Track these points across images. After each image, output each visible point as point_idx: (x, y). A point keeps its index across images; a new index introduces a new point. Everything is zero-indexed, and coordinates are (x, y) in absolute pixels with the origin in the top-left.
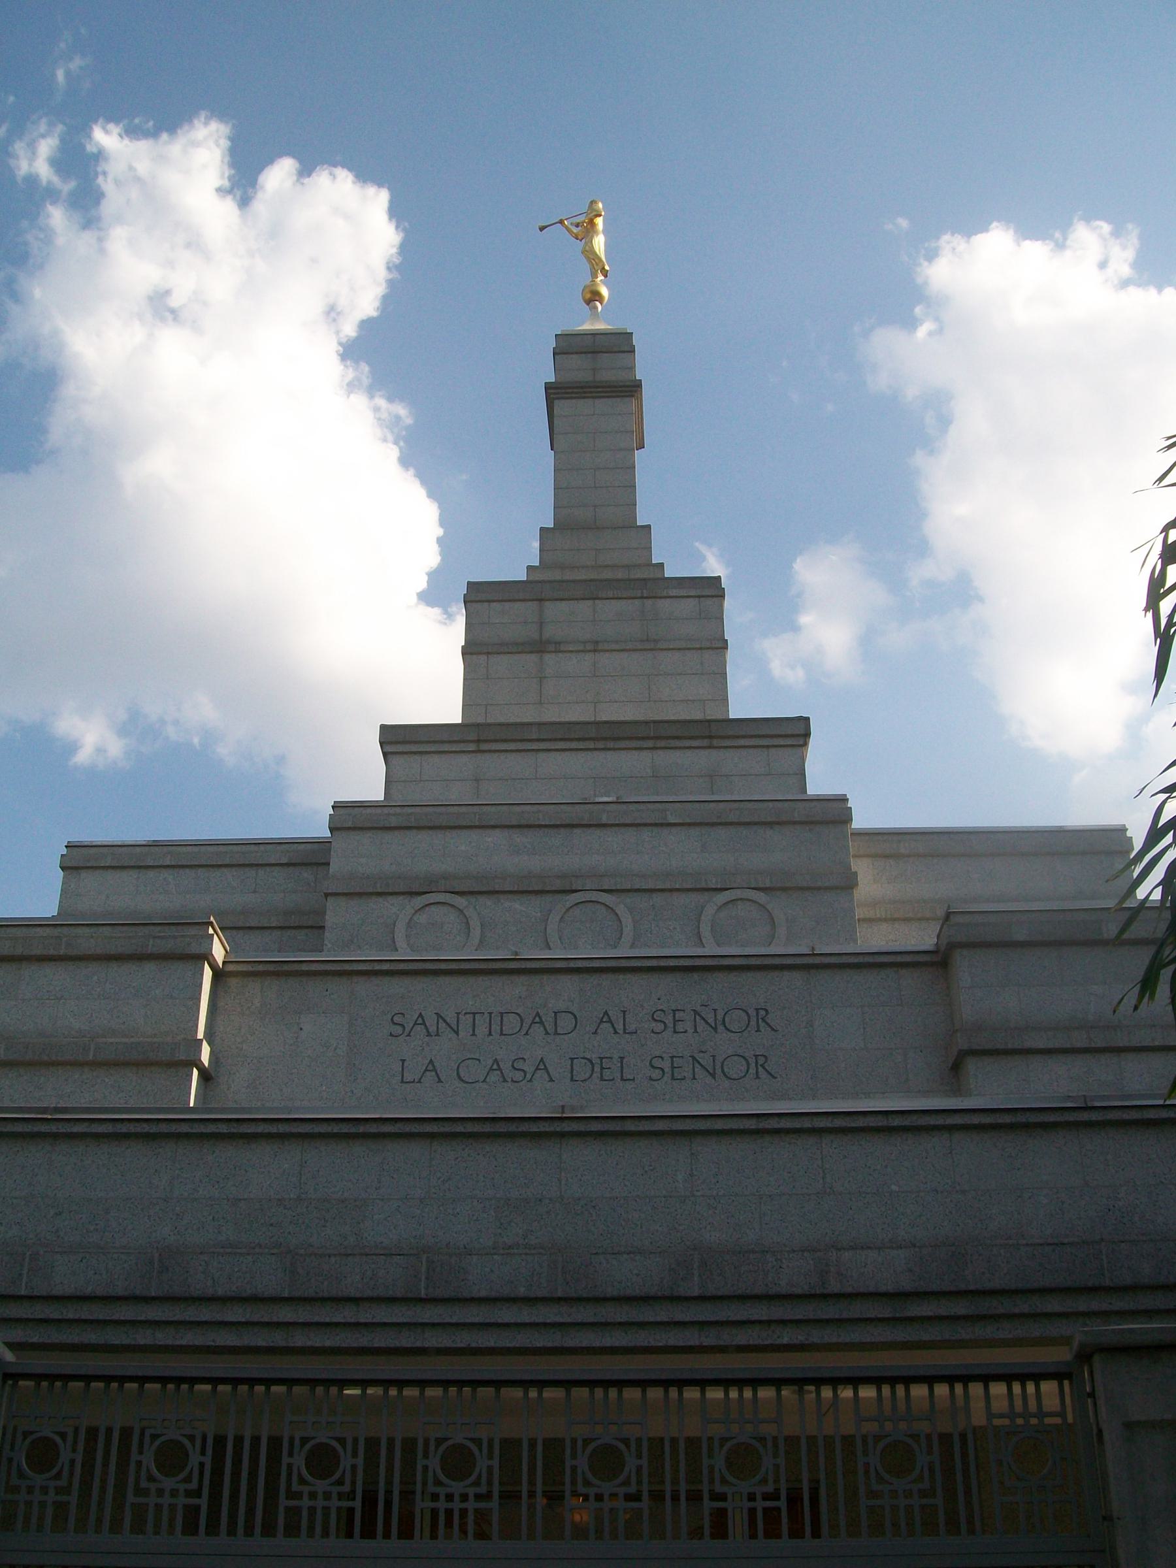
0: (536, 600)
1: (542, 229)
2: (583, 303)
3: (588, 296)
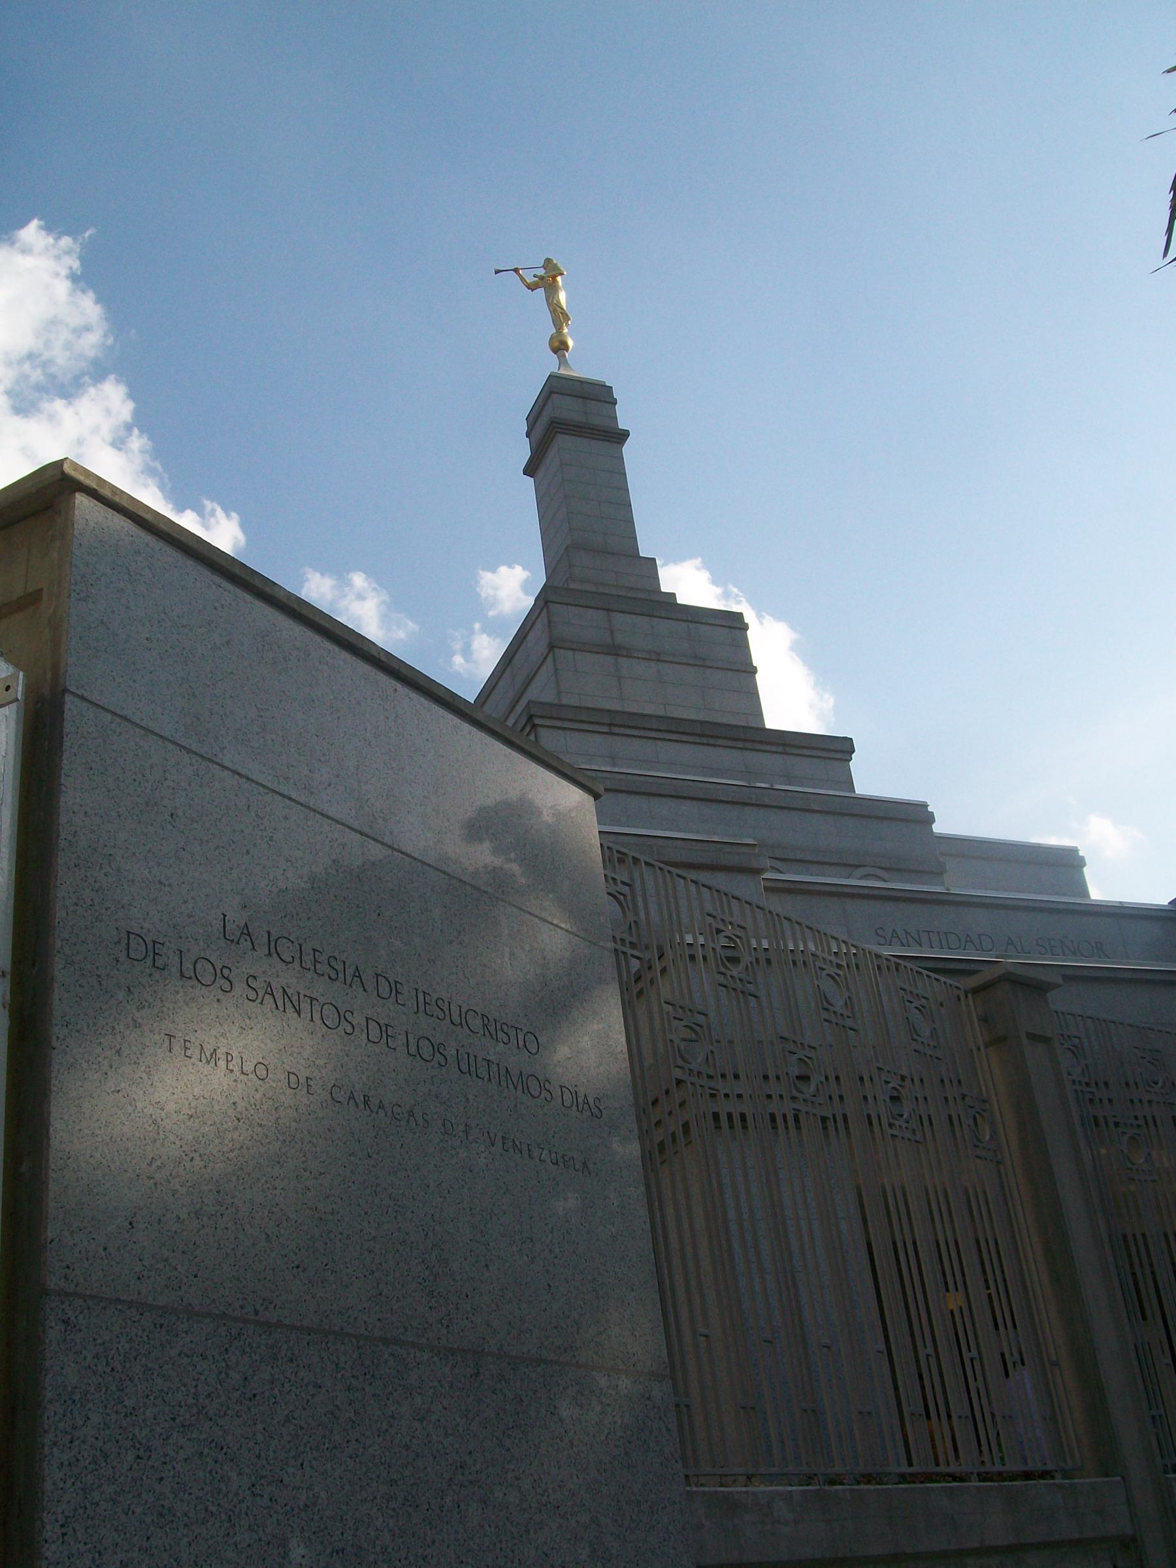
0: (604, 609)
1: (497, 272)
2: (551, 352)
3: (556, 344)
